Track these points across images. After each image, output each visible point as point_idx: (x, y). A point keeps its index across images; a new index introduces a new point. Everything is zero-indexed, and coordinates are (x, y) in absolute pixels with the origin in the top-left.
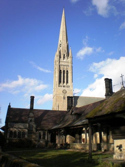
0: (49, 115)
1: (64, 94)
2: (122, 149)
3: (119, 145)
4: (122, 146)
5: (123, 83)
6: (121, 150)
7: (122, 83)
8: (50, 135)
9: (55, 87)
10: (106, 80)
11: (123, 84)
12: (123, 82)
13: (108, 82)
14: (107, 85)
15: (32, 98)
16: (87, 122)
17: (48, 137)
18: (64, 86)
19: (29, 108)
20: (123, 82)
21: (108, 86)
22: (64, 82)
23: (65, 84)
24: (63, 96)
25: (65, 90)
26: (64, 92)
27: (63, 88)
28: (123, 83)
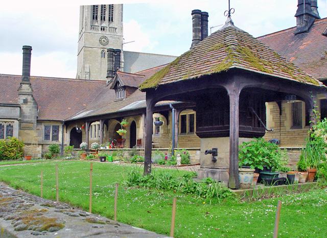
0: (158, 126)
1: (102, 46)
2: (216, 158)
3: (210, 149)
4: (218, 151)
5: (229, 13)
6: (214, 161)
7: (227, 12)
8: (68, 132)
9: (84, 31)
10: (195, 12)
11: (229, 16)
12: (230, 11)
13: (201, 18)
14: (197, 26)
15: (27, 51)
16: (143, 103)
17: (65, 139)
18: (103, 29)
19: (18, 71)
20: (230, 11)
21: (198, 27)
22: (103, 19)
23: (105, 24)
24: (100, 51)
25: (105, 37)
26: (103, 41)
27: (100, 32)
28: (229, 13)
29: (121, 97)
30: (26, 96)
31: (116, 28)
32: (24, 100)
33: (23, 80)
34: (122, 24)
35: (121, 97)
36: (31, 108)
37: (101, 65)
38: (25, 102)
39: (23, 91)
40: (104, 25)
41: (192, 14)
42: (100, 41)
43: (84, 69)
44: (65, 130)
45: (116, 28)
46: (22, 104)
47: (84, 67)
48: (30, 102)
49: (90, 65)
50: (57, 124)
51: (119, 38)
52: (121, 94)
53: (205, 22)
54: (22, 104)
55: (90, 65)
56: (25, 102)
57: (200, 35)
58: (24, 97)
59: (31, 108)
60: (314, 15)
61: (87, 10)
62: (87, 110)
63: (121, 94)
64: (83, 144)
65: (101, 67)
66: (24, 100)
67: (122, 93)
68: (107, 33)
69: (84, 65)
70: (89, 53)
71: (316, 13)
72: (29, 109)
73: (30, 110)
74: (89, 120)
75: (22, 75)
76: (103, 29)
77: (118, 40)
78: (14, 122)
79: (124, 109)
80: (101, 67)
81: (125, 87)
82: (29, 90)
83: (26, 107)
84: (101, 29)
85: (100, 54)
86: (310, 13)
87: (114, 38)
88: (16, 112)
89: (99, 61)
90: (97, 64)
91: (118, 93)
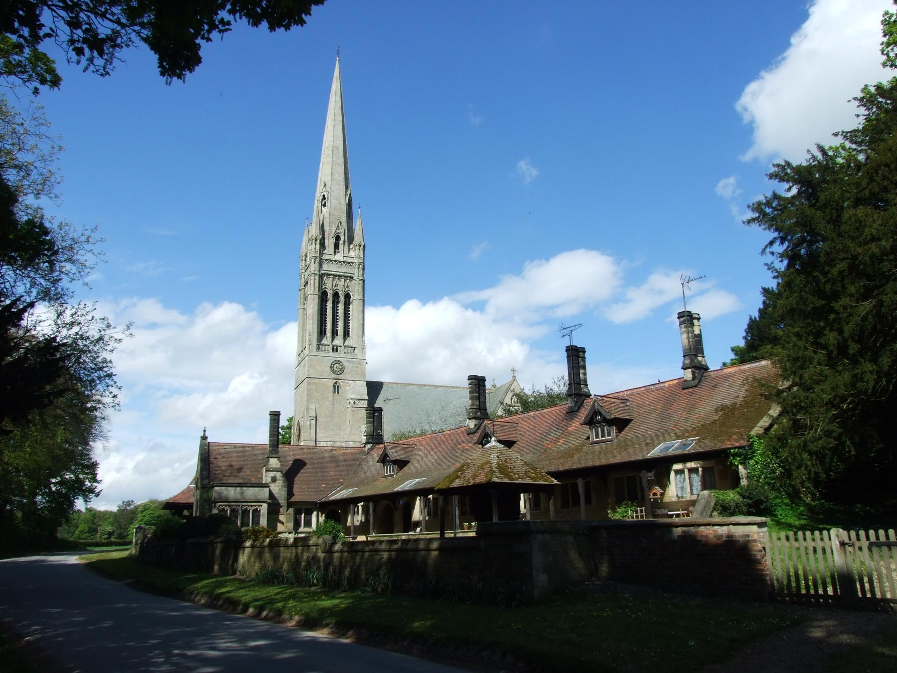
1: (334, 376)
9: (306, 352)
18: (335, 349)
24: (331, 383)
25: (338, 362)
27: (331, 354)
29: (390, 472)
30: (275, 472)
31: (355, 348)
32: (272, 477)
33: (271, 452)
34: (363, 341)
35: (390, 472)
36: (280, 488)
37: (333, 404)
38: (274, 480)
39: (271, 466)
40: (336, 342)
41: (468, 380)
42: (331, 367)
43: (308, 413)
44: (320, 513)
45: (355, 348)
46: (270, 483)
47: (308, 409)
48: (280, 480)
49: (317, 405)
50: (310, 507)
51: (359, 363)
52: (390, 469)
53: (481, 388)
54: (270, 483)
55: (317, 405)
56: (274, 480)
57: (478, 403)
58: (272, 474)
59: (280, 488)
60: (584, 393)
61: (311, 322)
62: (347, 488)
63: (390, 469)
64: (799, 471)
65: (333, 408)
66: (272, 477)
67: (392, 468)
68: (340, 356)
69: (308, 405)
70: (314, 387)
71: (587, 391)
72: (278, 488)
73: (279, 490)
74: (354, 501)
75: (267, 442)
76: (335, 349)
77: (358, 365)
78: (261, 506)
79: (398, 489)
80: (333, 408)
81: (395, 462)
82: (277, 465)
83: (275, 486)
84: (333, 350)
85: (332, 389)
86: (580, 393)
87: (353, 363)
88: (264, 493)
89: (331, 399)
90: (327, 403)
91: (387, 467)
